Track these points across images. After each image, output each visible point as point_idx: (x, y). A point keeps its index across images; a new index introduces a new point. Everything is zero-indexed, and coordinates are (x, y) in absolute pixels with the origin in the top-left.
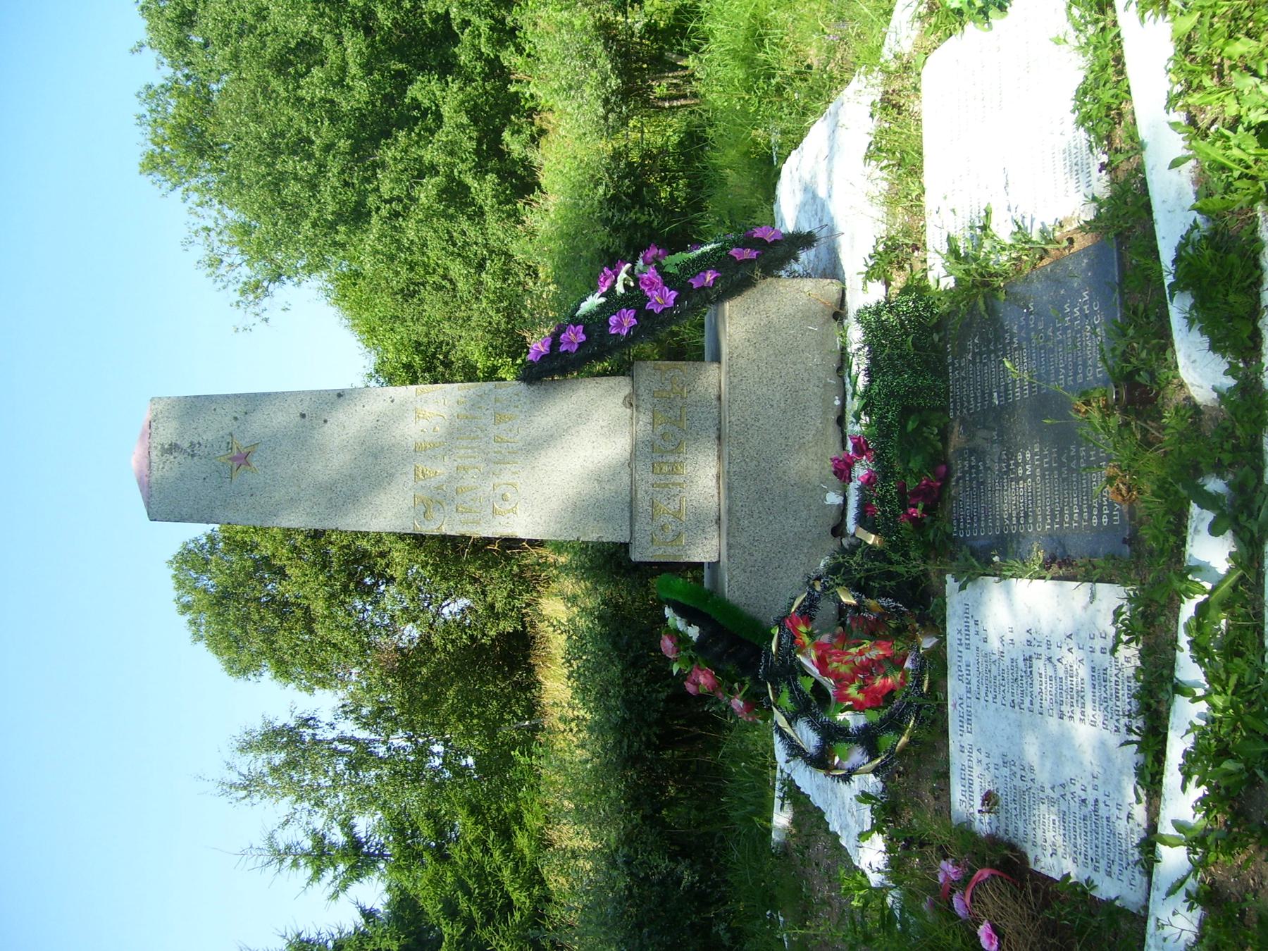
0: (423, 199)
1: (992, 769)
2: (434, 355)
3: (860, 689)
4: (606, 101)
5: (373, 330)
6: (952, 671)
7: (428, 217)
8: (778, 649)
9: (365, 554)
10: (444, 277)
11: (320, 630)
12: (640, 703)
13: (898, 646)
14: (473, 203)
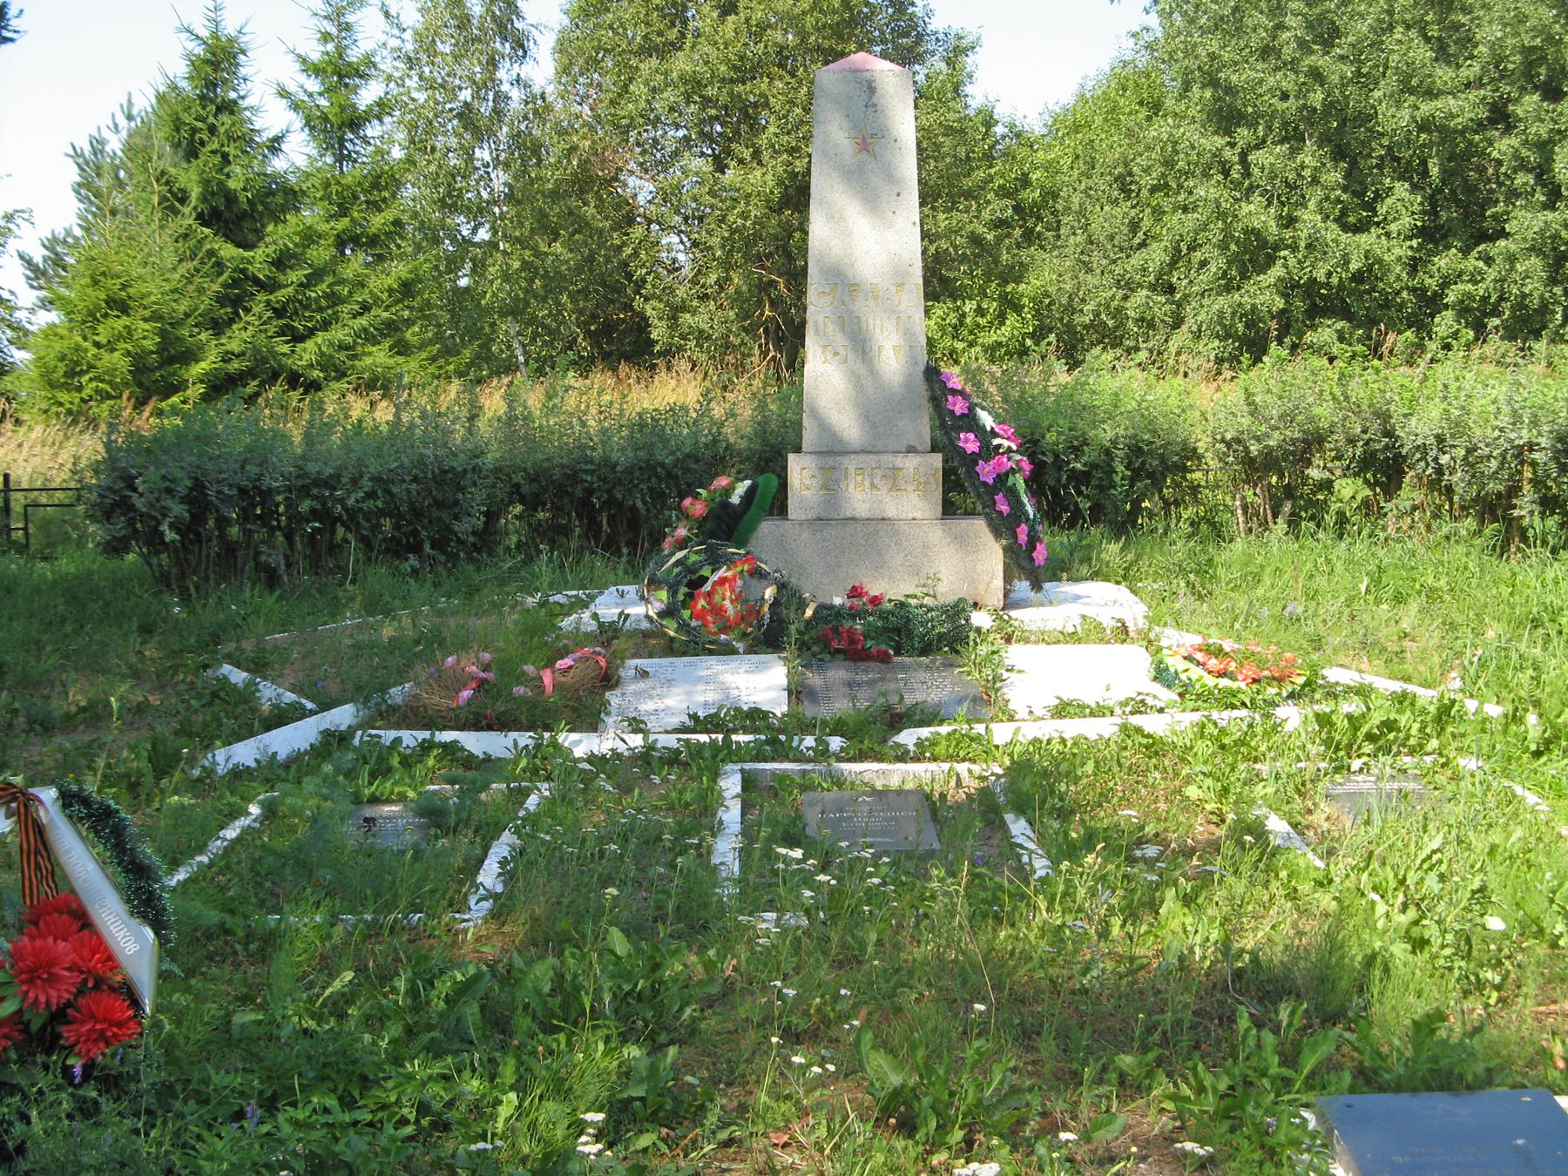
0: (1246, 208)
4: (1238, 441)
5: (1077, 128)
7: (1221, 215)
9: (756, 129)
11: (649, 65)
14: (1244, 276)
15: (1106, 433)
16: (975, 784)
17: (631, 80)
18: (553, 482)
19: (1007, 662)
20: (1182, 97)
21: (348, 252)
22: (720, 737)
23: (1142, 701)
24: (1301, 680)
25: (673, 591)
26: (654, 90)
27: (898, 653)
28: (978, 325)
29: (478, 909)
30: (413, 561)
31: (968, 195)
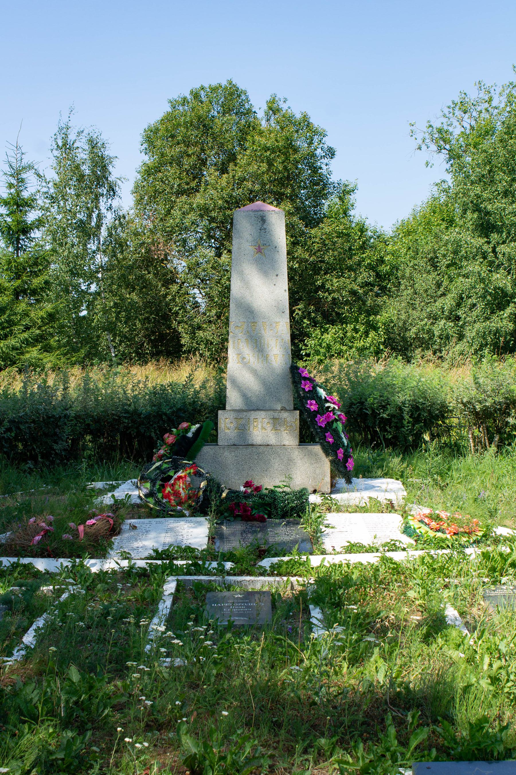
4: (469, 402)
5: (409, 233)
15: (400, 398)
16: (300, 588)
17: (172, 208)
18: (108, 423)
19: (326, 522)
20: (462, 217)
21: (20, 298)
22: (168, 561)
23: (394, 544)
24: (480, 534)
25: (154, 485)
26: (184, 213)
27: (270, 517)
28: (354, 338)
29: (18, 655)
30: (30, 464)
31: (350, 269)
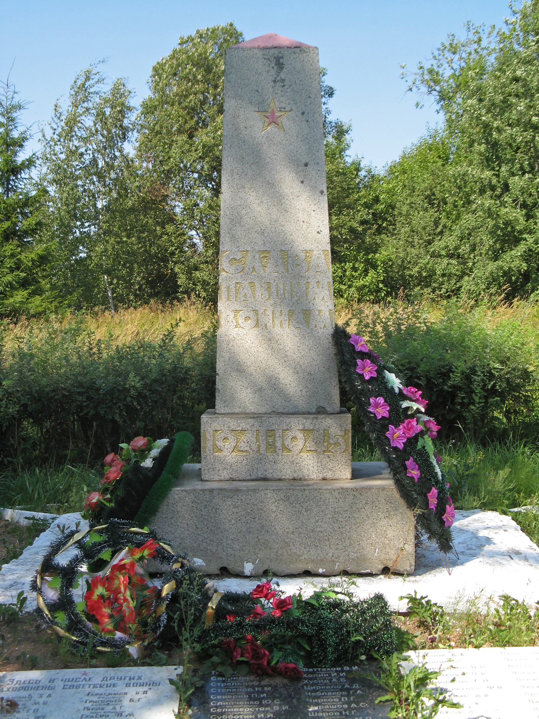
1: (35, 707)
2: (385, 219)
3: (101, 597)
6: (111, 672)
8: (132, 533)
10: (445, 227)
12: (111, 400)
13: (133, 627)
28: (353, 276)
31: (349, 207)
